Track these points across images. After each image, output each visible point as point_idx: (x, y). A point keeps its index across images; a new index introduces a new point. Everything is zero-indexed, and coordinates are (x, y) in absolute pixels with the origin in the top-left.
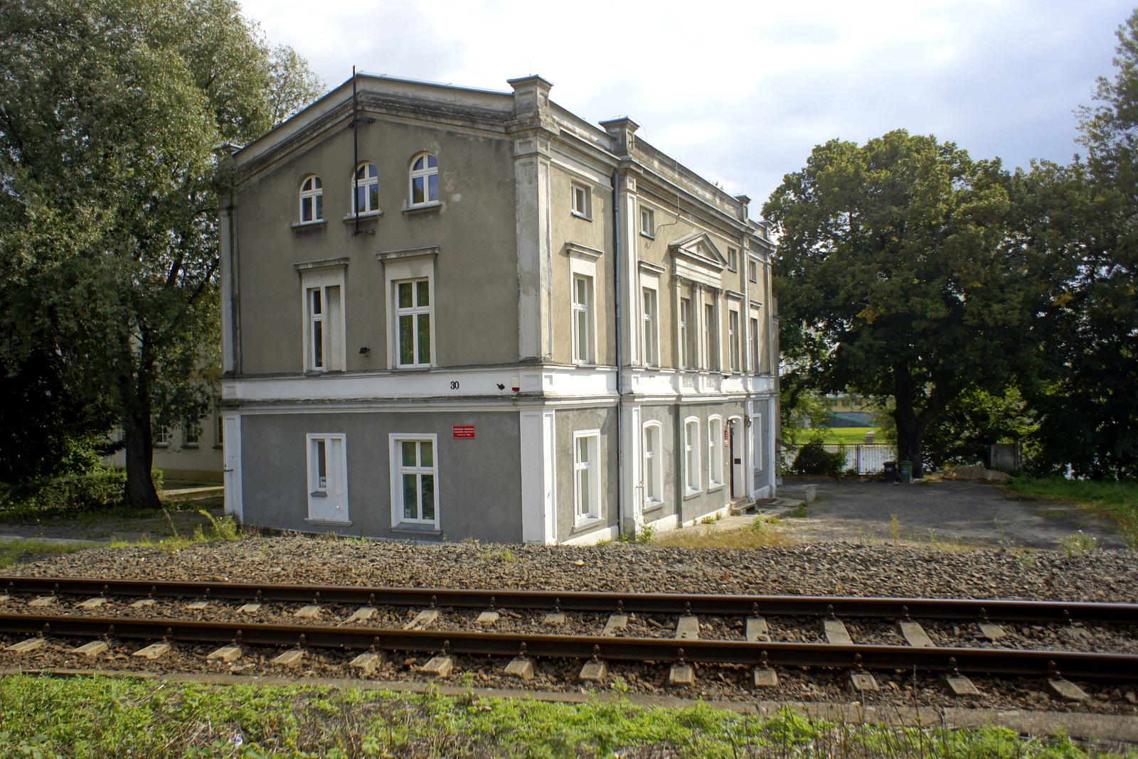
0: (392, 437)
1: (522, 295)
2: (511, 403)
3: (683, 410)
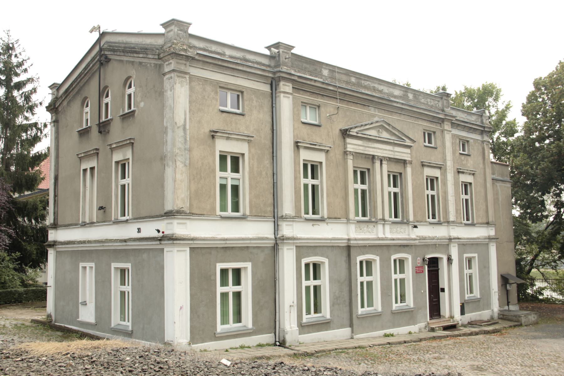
0: (114, 265)
1: (166, 167)
2: (158, 242)
3: (353, 251)
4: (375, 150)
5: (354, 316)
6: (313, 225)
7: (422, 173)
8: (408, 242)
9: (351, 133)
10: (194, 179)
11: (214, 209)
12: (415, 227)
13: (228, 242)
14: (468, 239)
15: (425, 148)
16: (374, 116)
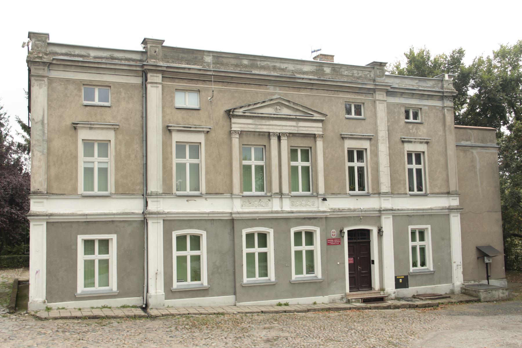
3: (235, 223)
4: (271, 127)
5: (238, 285)
6: (187, 201)
7: (342, 146)
8: (314, 214)
9: (235, 113)
10: (54, 165)
11: (75, 189)
12: (325, 199)
13: (88, 217)
14: (414, 210)
15: (347, 120)
16: (273, 94)
